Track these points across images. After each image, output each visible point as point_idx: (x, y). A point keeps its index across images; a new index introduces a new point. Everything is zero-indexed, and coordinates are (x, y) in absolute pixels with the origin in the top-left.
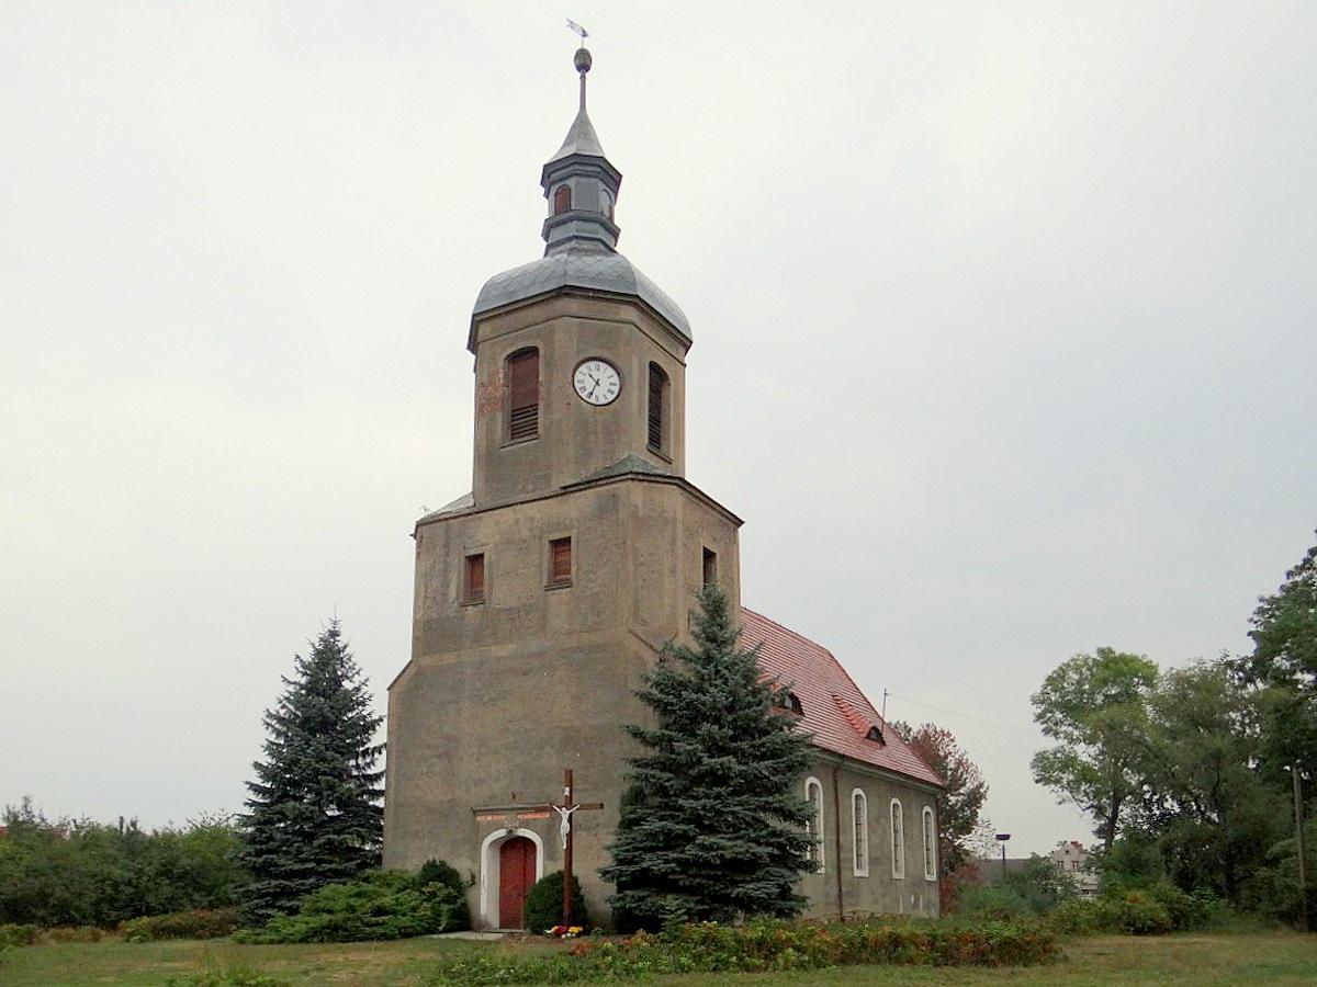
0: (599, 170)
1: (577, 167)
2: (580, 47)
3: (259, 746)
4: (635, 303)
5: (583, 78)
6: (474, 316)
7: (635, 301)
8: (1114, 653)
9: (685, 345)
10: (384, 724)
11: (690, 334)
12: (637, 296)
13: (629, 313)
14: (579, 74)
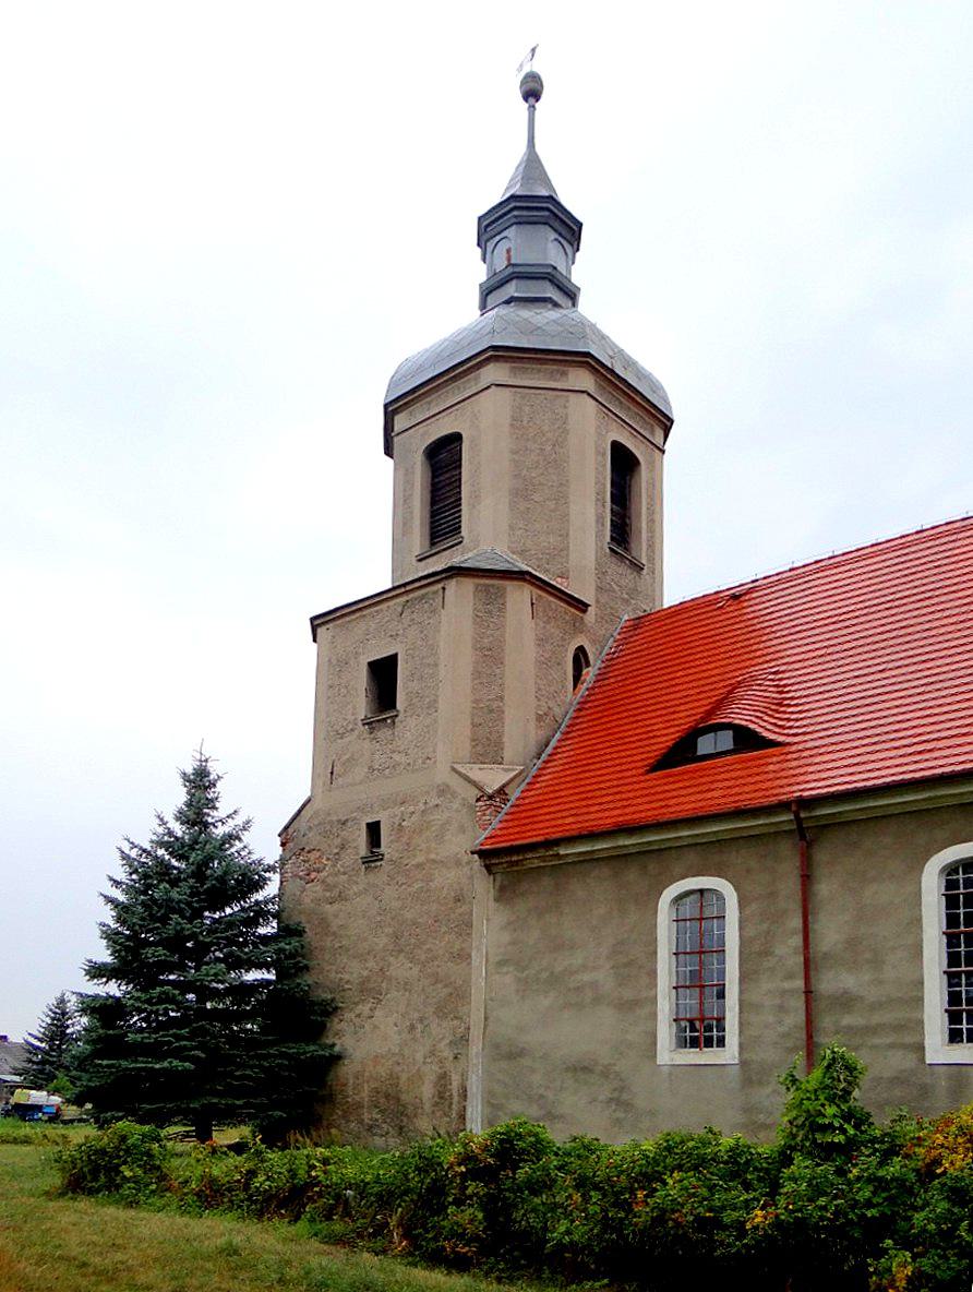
0: (547, 213)
1: (515, 213)
2: (528, 70)
3: (94, 924)
4: (588, 363)
7: (585, 360)
9: (666, 426)
12: (588, 354)
13: (583, 379)
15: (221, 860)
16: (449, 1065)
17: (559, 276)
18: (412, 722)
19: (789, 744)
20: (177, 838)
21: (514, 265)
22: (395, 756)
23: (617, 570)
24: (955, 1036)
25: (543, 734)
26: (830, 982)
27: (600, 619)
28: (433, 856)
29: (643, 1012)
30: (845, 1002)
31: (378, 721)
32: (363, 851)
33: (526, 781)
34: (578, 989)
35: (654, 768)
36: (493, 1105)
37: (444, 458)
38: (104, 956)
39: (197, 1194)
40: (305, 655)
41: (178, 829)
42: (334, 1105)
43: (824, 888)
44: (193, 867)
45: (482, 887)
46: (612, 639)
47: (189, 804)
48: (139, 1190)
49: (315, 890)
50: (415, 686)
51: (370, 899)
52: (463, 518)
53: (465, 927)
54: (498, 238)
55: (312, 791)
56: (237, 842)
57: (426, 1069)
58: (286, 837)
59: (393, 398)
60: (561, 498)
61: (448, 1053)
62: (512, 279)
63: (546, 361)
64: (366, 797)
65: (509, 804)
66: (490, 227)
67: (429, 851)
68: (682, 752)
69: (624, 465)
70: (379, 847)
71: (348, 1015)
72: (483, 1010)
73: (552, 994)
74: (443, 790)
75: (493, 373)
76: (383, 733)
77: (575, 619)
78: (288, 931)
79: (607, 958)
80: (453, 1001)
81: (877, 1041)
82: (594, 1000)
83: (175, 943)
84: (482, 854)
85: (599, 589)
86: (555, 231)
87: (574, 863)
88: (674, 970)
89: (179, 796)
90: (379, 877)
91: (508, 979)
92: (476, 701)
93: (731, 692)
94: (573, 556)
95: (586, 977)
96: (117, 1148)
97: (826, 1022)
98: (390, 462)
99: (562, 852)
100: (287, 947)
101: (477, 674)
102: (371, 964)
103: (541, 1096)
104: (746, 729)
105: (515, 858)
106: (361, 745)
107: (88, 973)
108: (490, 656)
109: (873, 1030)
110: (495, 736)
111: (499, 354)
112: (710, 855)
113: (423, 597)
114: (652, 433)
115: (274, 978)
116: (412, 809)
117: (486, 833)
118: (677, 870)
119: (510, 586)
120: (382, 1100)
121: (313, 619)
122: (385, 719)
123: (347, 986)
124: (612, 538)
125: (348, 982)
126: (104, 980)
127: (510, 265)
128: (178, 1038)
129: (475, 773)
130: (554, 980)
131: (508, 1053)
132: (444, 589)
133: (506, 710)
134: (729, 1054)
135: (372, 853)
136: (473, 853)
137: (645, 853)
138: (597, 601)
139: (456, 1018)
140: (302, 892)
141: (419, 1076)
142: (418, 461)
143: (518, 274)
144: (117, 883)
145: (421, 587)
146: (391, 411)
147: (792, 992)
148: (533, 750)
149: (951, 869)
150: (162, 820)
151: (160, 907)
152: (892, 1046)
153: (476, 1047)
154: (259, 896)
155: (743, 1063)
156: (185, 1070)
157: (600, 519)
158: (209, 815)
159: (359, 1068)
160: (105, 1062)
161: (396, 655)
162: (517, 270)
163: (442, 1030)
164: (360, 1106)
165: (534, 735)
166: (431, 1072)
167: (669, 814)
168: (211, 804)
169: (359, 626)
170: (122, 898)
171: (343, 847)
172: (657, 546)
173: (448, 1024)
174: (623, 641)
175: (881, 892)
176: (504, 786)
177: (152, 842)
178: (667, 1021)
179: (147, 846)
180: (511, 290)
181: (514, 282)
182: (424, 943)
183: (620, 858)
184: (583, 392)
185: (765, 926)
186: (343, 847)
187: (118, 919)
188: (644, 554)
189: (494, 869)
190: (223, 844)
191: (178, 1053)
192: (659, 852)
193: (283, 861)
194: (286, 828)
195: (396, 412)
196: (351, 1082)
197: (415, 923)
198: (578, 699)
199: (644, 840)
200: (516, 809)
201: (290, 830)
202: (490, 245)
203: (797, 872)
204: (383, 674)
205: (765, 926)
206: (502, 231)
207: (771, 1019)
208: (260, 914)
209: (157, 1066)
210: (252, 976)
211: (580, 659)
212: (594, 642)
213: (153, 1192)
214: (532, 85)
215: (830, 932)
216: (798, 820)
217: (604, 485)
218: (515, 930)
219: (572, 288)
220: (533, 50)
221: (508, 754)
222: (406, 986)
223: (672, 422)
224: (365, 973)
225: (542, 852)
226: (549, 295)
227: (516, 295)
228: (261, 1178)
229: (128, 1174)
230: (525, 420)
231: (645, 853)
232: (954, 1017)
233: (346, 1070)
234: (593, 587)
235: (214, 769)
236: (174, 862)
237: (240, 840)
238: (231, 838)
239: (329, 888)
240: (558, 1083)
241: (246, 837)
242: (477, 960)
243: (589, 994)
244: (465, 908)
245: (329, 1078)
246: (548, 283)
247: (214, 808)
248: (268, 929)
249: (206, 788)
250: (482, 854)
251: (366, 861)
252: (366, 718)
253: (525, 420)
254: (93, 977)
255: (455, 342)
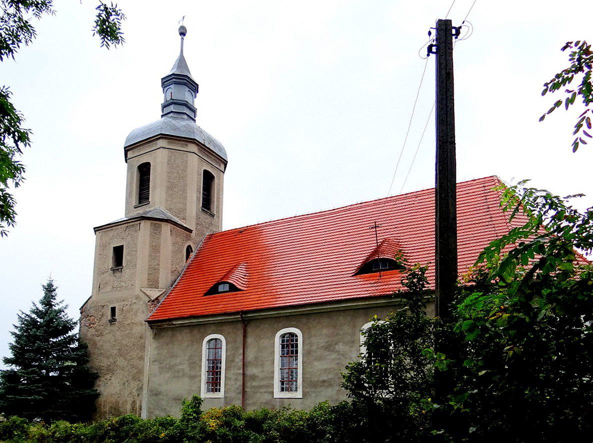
0: (186, 81)
1: (174, 80)
2: (182, 25)
5: (183, 39)
6: (125, 148)
7: (194, 141)
8: (172, 423)
10: (78, 326)
11: (225, 154)
12: (195, 139)
13: (193, 148)
14: (180, 37)
15: (57, 320)
16: (136, 397)
17: (189, 105)
18: (128, 271)
19: (242, 290)
20: (40, 311)
21: (173, 99)
22: (121, 283)
23: (205, 217)
24: (282, 390)
25: (173, 278)
26: (251, 371)
27: (197, 235)
28: (133, 321)
29: (197, 380)
30: (254, 377)
31: (117, 269)
32: (109, 318)
33: (167, 295)
34: (178, 371)
35: (206, 294)
36: (150, 412)
37: (144, 171)
38: (10, 355)
39: (37, 439)
40: (91, 240)
41: (41, 307)
42: (96, 412)
43: (249, 340)
44: (45, 323)
45: (149, 333)
46: (201, 242)
47: (45, 298)
48: (19, 439)
49: (92, 331)
50: (129, 258)
51: (111, 336)
52: (150, 194)
53: (143, 348)
54: (168, 87)
55: (92, 294)
56: (63, 313)
57: (128, 399)
58: (82, 310)
59: (128, 145)
60: (184, 191)
61: (136, 394)
62: (171, 104)
63: (180, 140)
64: (111, 297)
65: (160, 303)
66: (167, 82)
67: (132, 319)
68: (213, 290)
69: (208, 179)
70: (115, 316)
71: (102, 379)
72: (147, 378)
73: (170, 373)
74: (137, 297)
75: (162, 143)
76: (118, 274)
77: (187, 235)
78: (83, 346)
79: (187, 360)
80: (138, 375)
81: (262, 390)
82: (183, 375)
83: (38, 351)
84: (149, 322)
85: (197, 224)
86: (188, 87)
87: (178, 327)
88: (207, 365)
89: (42, 294)
90: (115, 328)
91: (156, 367)
92: (150, 265)
93: (232, 269)
94: (188, 212)
95: (181, 367)
96: (12, 426)
97: (248, 384)
98: (126, 164)
99: (174, 323)
100: (80, 353)
101: (150, 256)
102: (111, 360)
103: (165, 409)
104: (232, 284)
105: (159, 324)
106: (109, 276)
107: (4, 361)
108: (155, 249)
109: (260, 387)
110: (156, 279)
111: (163, 136)
112: (219, 326)
113: (133, 225)
114: (220, 166)
115: (76, 364)
116: (127, 303)
117: (151, 314)
118: (209, 332)
119: (163, 224)
120: (113, 411)
121: (162, 79)
122: (118, 269)
123: (102, 368)
124: (203, 206)
125: (103, 366)
126: (10, 364)
127: (171, 99)
128: (38, 387)
129: (148, 292)
130: (171, 368)
131: (155, 393)
132: (140, 223)
133: (160, 269)
134: (221, 394)
135: (113, 318)
136: (145, 321)
137: (199, 325)
138: (196, 228)
139: (139, 381)
140: (87, 332)
141: (126, 401)
142: (136, 169)
143: (174, 102)
144: (16, 327)
145: (133, 222)
146: (127, 150)
147: (240, 374)
148: (169, 283)
149: (283, 336)
150: (34, 304)
151: (33, 337)
152: (265, 392)
153: (145, 392)
154: (70, 333)
155: (225, 397)
156: (40, 399)
157: (198, 199)
158: (52, 302)
159: (105, 399)
160: (10, 396)
161: (123, 246)
162: (174, 101)
163: (134, 385)
164: (105, 412)
165: (170, 278)
166: (130, 401)
167: (206, 313)
168: (53, 297)
169: (112, 233)
170: (18, 333)
171: (102, 315)
172: (220, 207)
173: (136, 383)
174: (205, 243)
175: (265, 342)
176: (158, 297)
177: (31, 311)
178: (204, 384)
179: (28, 313)
180: (172, 108)
181: (173, 105)
182: (129, 353)
183: (191, 327)
184: (193, 152)
185: (233, 352)
186: (102, 315)
187: (16, 342)
188: (215, 211)
189: (154, 327)
190: (58, 313)
191: (39, 394)
192: (204, 325)
193: (80, 320)
194: (82, 307)
195: (128, 150)
196: (103, 404)
197: (126, 346)
198: (187, 264)
199: (199, 321)
200: (159, 308)
201: (84, 308)
202: (166, 89)
203: (242, 334)
204: (118, 252)
205: (233, 352)
206: (170, 85)
207: (233, 383)
208: (72, 339)
209: (30, 398)
210: (69, 363)
211: (189, 250)
212: (194, 243)
213: (24, 439)
214: (182, 31)
215: (251, 355)
216: (242, 317)
217: (200, 186)
218: (159, 350)
219: (194, 109)
220: (183, 17)
221: (160, 285)
222: (123, 369)
223: (227, 162)
224: (109, 363)
225: (168, 323)
226: (185, 112)
227: (173, 110)
228: (57, 433)
229: (16, 433)
230: (172, 161)
231: (199, 325)
232: (282, 383)
233: (102, 399)
234: (195, 223)
235: (55, 285)
236: (38, 320)
237: (64, 312)
238: (60, 311)
239: (97, 331)
240: (170, 405)
241: (66, 311)
242: (147, 360)
243: (181, 374)
244: (143, 341)
245: (96, 402)
246: (185, 107)
247: (55, 299)
248: (75, 345)
249: (51, 291)
250: (149, 322)
251: (111, 321)
252: (112, 268)
253: (172, 161)
254: (6, 363)
255: (149, 128)
